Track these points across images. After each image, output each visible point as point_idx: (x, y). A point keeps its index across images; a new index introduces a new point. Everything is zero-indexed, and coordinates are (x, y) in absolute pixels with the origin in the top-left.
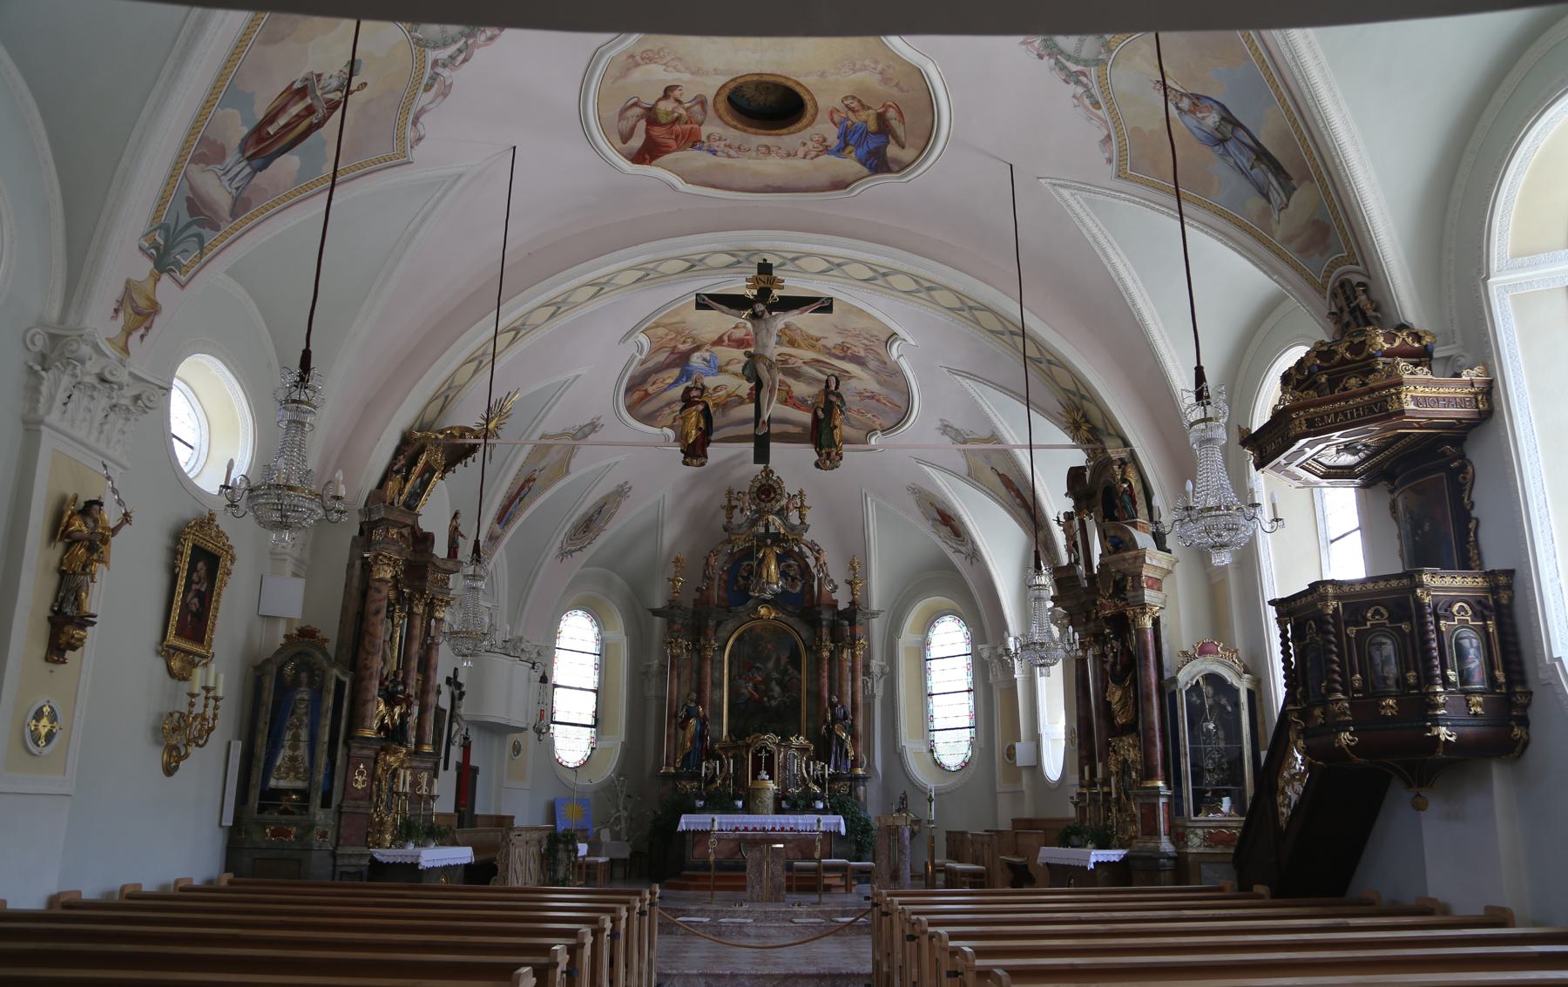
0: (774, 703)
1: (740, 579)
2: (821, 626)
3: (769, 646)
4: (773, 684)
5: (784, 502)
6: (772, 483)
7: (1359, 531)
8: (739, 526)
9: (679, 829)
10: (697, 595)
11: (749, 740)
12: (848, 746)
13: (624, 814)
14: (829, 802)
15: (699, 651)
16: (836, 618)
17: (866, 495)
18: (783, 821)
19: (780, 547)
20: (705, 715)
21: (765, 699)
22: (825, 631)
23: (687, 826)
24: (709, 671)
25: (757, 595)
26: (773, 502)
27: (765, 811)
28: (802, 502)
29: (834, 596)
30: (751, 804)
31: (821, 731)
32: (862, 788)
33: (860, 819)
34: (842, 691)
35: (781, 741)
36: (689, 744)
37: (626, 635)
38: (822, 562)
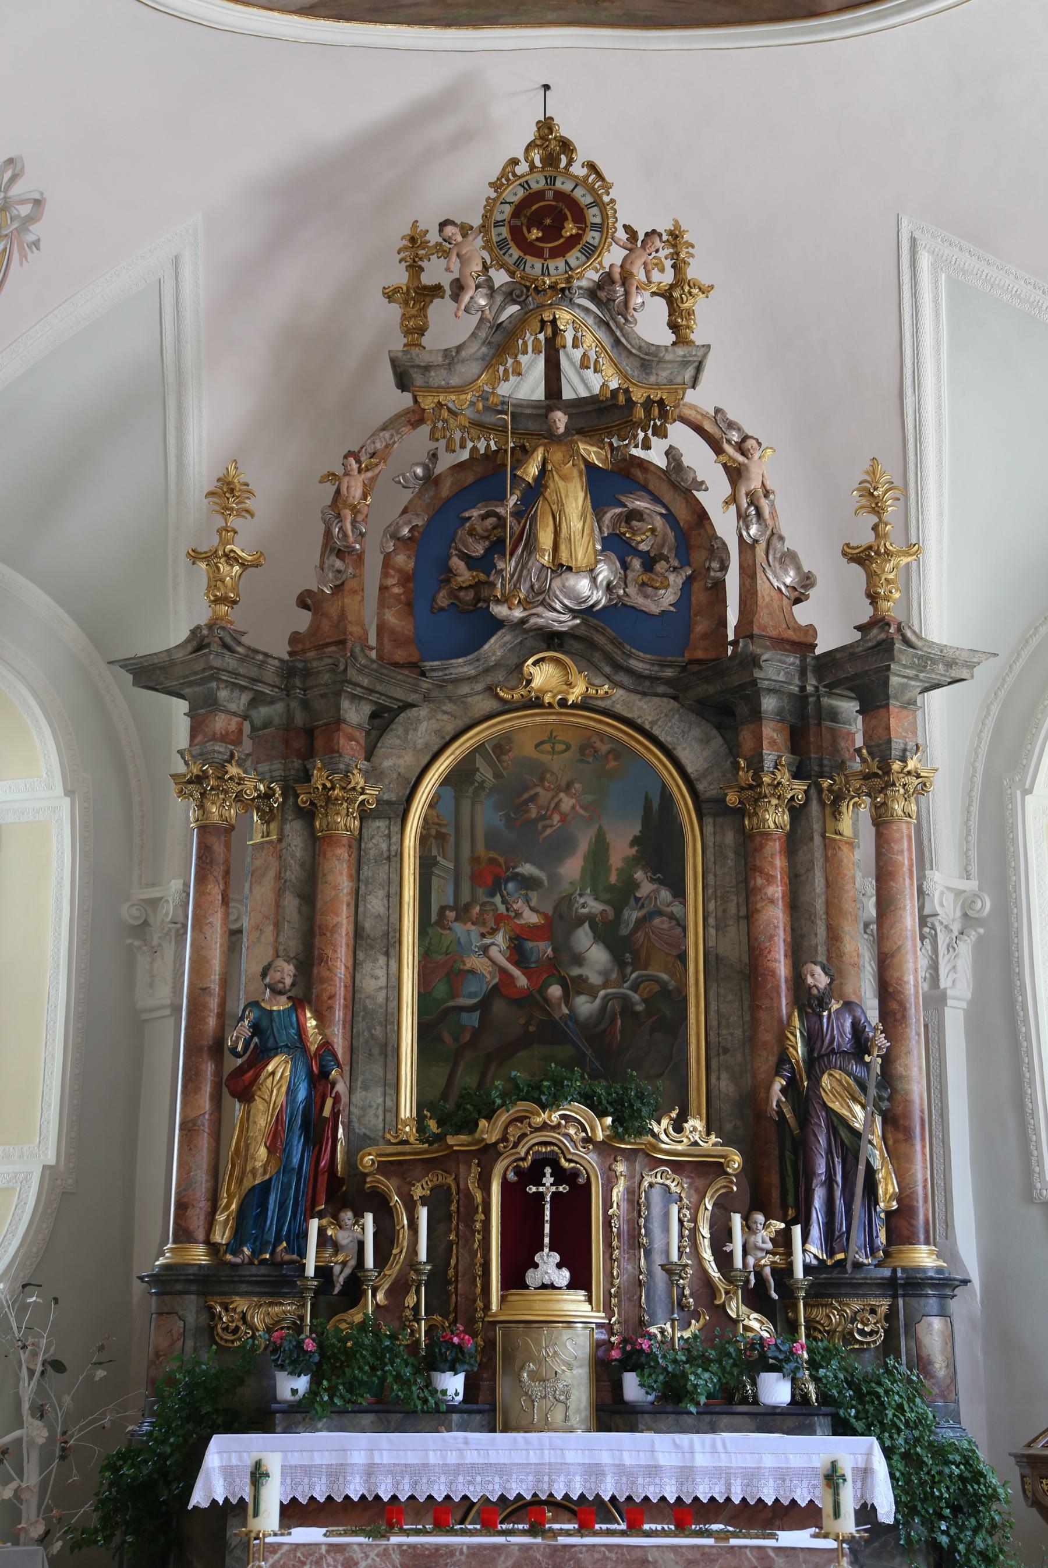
0: (585, 1006)
1: (457, 564)
2: (756, 715)
3: (567, 803)
4: (583, 938)
5: (613, 256)
6: (567, 187)
7: (829, 1418)
8: (452, 357)
9: (199, 1498)
10: (303, 620)
11: (489, 1131)
12: (876, 1155)
13: (36, 1432)
14: (816, 1379)
15: (308, 815)
16: (811, 682)
17: (913, 241)
18: (628, 1459)
19: (600, 444)
20: (326, 1046)
21: (555, 991)
22: (772, 733)
23: (229, 1485)
24: (345, 885)
25: (518, 613)
26: (574, 257)
27: (557, 1416)
28: (678, 268)
29: (802, 614)
30: (503, 1388)
31: (768, 1099)
32: (937, 1323)
33: (940, 1452)
34: (840, 956)
35: (617, 1133)
36: (262, 1152)
37: (69, 792)
38: (755, 484)
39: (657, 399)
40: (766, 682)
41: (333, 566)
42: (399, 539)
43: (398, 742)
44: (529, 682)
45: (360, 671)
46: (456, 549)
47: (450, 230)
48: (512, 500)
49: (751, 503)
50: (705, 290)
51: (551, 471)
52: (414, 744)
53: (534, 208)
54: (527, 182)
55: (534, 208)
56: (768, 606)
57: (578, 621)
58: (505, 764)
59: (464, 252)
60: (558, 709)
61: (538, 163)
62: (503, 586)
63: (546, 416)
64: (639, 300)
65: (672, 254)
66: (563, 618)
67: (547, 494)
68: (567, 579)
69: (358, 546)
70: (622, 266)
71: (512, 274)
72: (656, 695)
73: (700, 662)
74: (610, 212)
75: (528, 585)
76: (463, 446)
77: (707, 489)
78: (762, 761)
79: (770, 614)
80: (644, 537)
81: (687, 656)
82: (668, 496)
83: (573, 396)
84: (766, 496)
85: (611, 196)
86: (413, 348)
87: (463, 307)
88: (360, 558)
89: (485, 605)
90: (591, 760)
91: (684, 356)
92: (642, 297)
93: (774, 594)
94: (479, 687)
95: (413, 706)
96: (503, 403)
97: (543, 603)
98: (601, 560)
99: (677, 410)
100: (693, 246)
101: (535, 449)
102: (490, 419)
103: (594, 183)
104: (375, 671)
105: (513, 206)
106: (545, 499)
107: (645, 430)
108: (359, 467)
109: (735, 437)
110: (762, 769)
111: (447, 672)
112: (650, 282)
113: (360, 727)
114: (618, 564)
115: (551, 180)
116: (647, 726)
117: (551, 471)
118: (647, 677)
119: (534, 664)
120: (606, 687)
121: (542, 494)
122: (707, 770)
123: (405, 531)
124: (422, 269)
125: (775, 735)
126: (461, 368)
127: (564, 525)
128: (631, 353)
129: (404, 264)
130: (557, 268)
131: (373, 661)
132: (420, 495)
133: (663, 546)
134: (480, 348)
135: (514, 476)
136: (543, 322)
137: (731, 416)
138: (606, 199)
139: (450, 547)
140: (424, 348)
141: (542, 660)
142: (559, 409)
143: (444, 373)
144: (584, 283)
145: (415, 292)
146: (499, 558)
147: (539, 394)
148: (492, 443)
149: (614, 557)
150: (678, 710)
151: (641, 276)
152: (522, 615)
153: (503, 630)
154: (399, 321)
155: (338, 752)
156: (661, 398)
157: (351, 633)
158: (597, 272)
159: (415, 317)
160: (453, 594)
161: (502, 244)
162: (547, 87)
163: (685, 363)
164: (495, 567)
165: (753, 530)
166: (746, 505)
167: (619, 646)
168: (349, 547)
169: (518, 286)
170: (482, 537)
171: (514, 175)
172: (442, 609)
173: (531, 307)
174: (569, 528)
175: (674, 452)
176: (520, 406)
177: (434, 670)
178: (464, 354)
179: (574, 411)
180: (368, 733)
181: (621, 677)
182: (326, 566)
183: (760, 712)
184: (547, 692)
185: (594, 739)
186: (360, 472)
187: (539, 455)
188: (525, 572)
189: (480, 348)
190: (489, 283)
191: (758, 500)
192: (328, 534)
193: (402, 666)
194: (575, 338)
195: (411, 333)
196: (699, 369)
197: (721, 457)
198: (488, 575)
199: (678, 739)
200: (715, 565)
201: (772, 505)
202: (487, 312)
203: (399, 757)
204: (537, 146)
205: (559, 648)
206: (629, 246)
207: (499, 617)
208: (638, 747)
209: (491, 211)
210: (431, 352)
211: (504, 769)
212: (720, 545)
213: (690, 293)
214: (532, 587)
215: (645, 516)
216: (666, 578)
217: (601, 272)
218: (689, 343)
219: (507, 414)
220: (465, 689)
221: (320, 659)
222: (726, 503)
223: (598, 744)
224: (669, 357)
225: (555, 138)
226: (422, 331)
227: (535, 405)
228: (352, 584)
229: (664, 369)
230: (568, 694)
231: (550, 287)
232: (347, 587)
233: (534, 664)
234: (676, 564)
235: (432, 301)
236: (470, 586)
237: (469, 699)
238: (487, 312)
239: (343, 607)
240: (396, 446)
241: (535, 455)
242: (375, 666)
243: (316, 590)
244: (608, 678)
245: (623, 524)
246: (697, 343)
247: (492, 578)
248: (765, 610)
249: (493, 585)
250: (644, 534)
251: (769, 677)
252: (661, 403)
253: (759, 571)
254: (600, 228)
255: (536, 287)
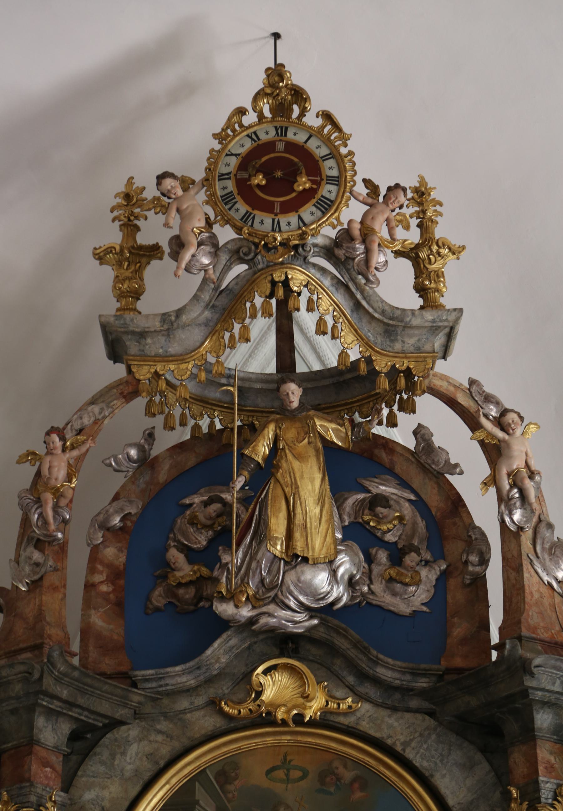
6: (301, 138)
25: (246, 612)
39: (404, 368)
40: (540, 693)
41: (30, 558)
42: (108, 529)
43: (102, 769)
44: (259, 694)
45: (58, 680)
46: (175, 540)
47: (168, 183)
48: (239, 482)
49: (514, 485)
50: (455, 251)
51: (283, 449)
52: (122, 770)
53: (264, 159)
54: (255, 133)
55: (264, 159)
56: (538, 603)
57: (316, 622)
58: (230, 795)
59: (185, 207)
60: (293, 727)
61: (267, 113)
62: (229, 580)
63: (278, 389)
64: (382, 259)
65: (418, 213)
66: (299, 617)
67: (279, 475)
68: (303, 572)
69: (60, 535)
70: (362, 223)
71: (238, 230)
72: (408, 710)
73: (459, 671)
74: (348, 165)
75: (257, 579)
76: (183, 424)
77: (461, 473)
78: (537, 789)
79: (541, 613)
80: (390, 526)
81: (444, 664)
82: (417, 480)
83: (306, 370)
84: (531, 477)
85: (349, 148)
86: (127, 312)
87: (183, 266)
88: (63, 548)
89: (207, 605)
90: (332, 790)
91: (434, 321)
92: (385, 255)
93: (545, 591)
94: (200, 700)
95: (121, 723)
96: (229, 377)
97: (275, 600)
98: (341, 551)
99: (426, 382)
100: (441, 204)
101: (265, 426)
102: (214, 394)
103: (330, 134)
104: (76, 680)
105: (240, 158)
106: (278, 481)
107: (389, 405)
108: (64, 445)
109: (494, 412)
110: (538, 800)
111: (162, 682)
112: (393, 239)
113: (56, 749)
114: (362, 556)
115: (282, 131)
116: (399, 748)
117: (283, 449)
118: (397, 689)
119: (265, 672)
120: (350, 700)
121: (273, 475)
122: (472, 802)
123: (116, 520)
124: (138, 229)
125: (552, 759)
126: (180, 334)
127: (299, 510)
128: (373, 317)
129: (117, 223)
130: (289, 224)
131: (74, 668)
132: (133, 479)
133: (412, 536)
134: (203, 312)
135: (241, 456)
136: (274, 283)
137: (488, 388)
138: (344, 151)
139: (168, 538)
140: (140, 313)
141: (274, 668)
142: (293, 381)
143: (162, 339)
144: (319, 240)
145: (130, 252)
146: (224, 551)
147: (271, 369)
148: (217, 421)
149: (356, 547)
150: (435, 729)
151: (384, 233)
152: (250, 614)
153: (229, 633)
154: (112, 284)
155: (29, 780)
156: (408, 368)
157: (50, 637)
158: (334, 227)
159: (130, 279)
160: (171, 592)
161: (228, 199)
162: (277, 36)
163: (434, 329)
164: (220, 560)
165: (517, 516)
166: (508, 487)
167: (365, 651)
168: (50, 536)
169: (245, 243)
170: (205, 527)
171: (241, 125)
172: (157, 610)
173: (260, 266)
174: (305, 514)
175: (423, 431)
176: (249, 380)
177: (147, 680)
178: (184, 318)
179: (309, 386)
180: (66, 757)
181: (368, 689)
182: (22, 558)
183: (533, 730)
184: (279, 706)
185: (336, 764)
186: (64, 449)
187: (271, 428)
188: (254, 565)
189: (203, 312)
190: (213, 241)
191: (522, 480)
192: (26, 522)
193: (110, 677)
194: (310, 301)
195: (125, 297)
196: (450, 336)
197: (478, 434)
198: (212, 570)
199: (436, 763)
200: (474, 558)
201: (538, 488)
202: (211, 272)
203: (104, 787)
204: (267, 95)
205: (295, 654)
206: (370, 200)
207: (224, 616)
208: (388, 773)
209: (216, 163)
210: (147, 316)
211: (229, 801)
212: (478, 536)
213: (439, 253)
214: (262, 581)
215: (392, 503)
216: (418, 573)
217: (339, 228)
218: (439, 307)
219: (233, 386)
220: (184, 703)
221: (11, 666)
222: (485, 484)
223: (341, 770)
224: (416, 322)
225: (287, 85)
226: (137, 295)
227: (265, 379)
228: (53, 579)
229: (411, 336)
230: (305, 709)
231: (281, 244)
232: (46, 582)
233: (266, 672)
234: (428, 556)
235: (149, 263)
236: (191, 583)
237: (189, 715)
238: (211, 272)
239: (40, 605)
240: (106, 421)
241: (266, 431)
242: (76, 674)
243: (9, 587)
244: (352, 690)
245: (367, 511)
246: (447, 307)
247: (216, 573)
248: (534, 608)
249: (217, 581)
250: (390, 522)
251: (543, 686)
252: (408, 373)
253: (525, 563)
254: (337, 181)
255: (266, 244)
